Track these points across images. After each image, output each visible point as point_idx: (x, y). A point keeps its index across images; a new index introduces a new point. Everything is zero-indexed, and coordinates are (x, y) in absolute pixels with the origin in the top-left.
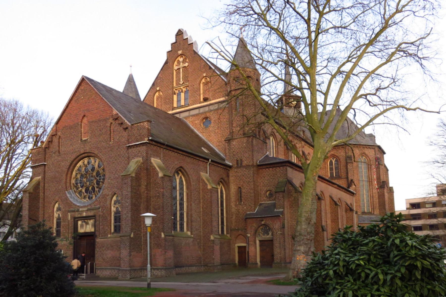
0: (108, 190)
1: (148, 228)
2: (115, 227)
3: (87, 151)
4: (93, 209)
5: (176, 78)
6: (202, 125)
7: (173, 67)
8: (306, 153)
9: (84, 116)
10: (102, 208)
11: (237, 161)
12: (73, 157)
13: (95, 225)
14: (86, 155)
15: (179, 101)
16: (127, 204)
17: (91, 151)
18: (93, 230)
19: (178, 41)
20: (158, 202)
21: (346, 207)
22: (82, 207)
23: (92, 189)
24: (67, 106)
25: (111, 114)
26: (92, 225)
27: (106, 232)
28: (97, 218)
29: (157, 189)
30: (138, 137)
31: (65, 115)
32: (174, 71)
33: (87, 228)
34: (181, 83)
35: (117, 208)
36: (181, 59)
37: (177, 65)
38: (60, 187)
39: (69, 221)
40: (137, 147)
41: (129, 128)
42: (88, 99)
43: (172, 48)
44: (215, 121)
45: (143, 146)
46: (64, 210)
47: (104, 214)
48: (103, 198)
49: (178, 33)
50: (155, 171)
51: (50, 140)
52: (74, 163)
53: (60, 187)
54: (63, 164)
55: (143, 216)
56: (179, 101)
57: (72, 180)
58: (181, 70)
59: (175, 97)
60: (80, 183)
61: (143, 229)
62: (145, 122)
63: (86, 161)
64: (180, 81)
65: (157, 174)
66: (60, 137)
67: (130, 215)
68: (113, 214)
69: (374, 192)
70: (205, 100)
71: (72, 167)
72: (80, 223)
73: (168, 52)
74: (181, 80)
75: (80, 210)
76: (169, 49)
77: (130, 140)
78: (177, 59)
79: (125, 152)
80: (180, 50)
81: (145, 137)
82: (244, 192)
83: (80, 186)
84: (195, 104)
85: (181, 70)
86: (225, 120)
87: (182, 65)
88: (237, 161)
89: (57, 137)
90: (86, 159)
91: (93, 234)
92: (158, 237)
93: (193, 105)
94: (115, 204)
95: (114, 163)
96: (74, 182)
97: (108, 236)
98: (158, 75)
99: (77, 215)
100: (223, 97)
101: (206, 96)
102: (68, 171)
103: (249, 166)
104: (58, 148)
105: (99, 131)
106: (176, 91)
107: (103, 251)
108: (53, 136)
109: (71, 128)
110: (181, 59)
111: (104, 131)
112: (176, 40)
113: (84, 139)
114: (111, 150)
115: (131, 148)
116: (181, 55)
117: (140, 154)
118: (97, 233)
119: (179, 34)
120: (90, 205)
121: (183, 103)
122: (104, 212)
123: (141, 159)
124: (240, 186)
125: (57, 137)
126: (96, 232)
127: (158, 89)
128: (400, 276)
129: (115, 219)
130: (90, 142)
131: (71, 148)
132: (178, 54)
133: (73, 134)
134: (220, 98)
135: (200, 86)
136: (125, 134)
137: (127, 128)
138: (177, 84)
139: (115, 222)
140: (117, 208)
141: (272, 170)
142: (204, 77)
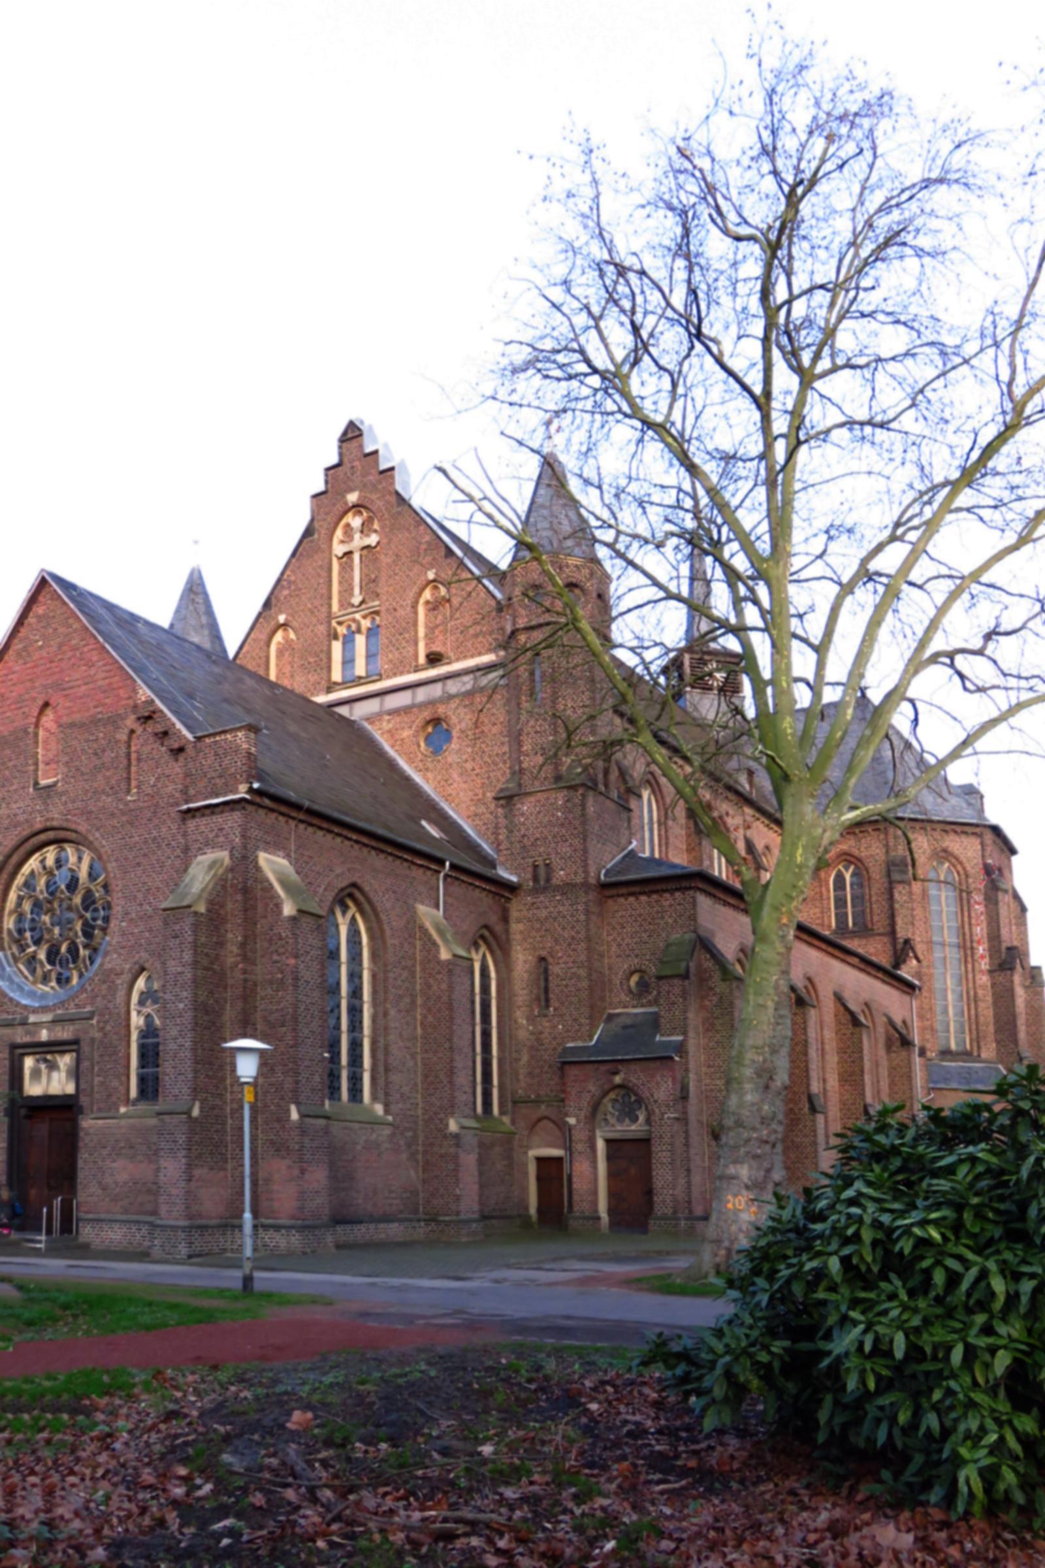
2: (142, 1080)
3: (55, 824)
6: (422, 744)
8: (759, 846)
9: (46, 705)
11: (536, 867)
13: (76, 1073)
15: (348, 662)
16: (181, 1006)
18: (70, 1089)
19: (345, 460)
21: (887, 1032)
22: (35, 1011)
23: (69, 950)
25: (131, 702)
26: (69, 1073)
27: (114, 1099)
28: (85, 1048)
29: (275, 957)
34: (356, 600)
37: (342, 542)
41: (190, 750)
42: (60, 646)
43: (326, 482)
44: (462, 731)
45: (232, 810)
48: (104, 982)
49: (345, 433)
56: (348, 662)
59: (337, 647)
62: (239, 729)
63: (50, 854)
64: (352, 595)
65: (278, 907)
67: (188, 1044)
68: (134, 1036)
70: (434, 659)
72: (29, 1062)
73: (315, 496)
74: (357, 590)
77: (192, 792)
80: (351, 490)
81: (237, 782)
83: (29, 941)
84: (402, 673)
85: (356, 557)
86: (495, 730)
87: (358, 541)
88: (536, 867)
90: (51, 848)
92: (278, 1120)
93: (395, 675)
94: (141, 1003)
97: (117, 1110)
98: (283, 574)
100: (489, 651)
101: (436, 648)
105: (94, 758)
107: (103, 1160)
110: (356, 522)
111: (109, 755)
112: (341, 455)
113: (44, 782)
114: (131, 823)
115: (194, 817)
116: (357, 507)
117: (221, 839)
118: (84, 1100)
120: (63, 1003)
121: (360, 669)
124: (544, 953)
127: (282, 619)
129: (142, 1056)
132: (346, 503)
133: (10, 764)
134: (480, 654)
135: (416, 613)
136: (176, 768)
137: (181, 750)
141: (649, 903)
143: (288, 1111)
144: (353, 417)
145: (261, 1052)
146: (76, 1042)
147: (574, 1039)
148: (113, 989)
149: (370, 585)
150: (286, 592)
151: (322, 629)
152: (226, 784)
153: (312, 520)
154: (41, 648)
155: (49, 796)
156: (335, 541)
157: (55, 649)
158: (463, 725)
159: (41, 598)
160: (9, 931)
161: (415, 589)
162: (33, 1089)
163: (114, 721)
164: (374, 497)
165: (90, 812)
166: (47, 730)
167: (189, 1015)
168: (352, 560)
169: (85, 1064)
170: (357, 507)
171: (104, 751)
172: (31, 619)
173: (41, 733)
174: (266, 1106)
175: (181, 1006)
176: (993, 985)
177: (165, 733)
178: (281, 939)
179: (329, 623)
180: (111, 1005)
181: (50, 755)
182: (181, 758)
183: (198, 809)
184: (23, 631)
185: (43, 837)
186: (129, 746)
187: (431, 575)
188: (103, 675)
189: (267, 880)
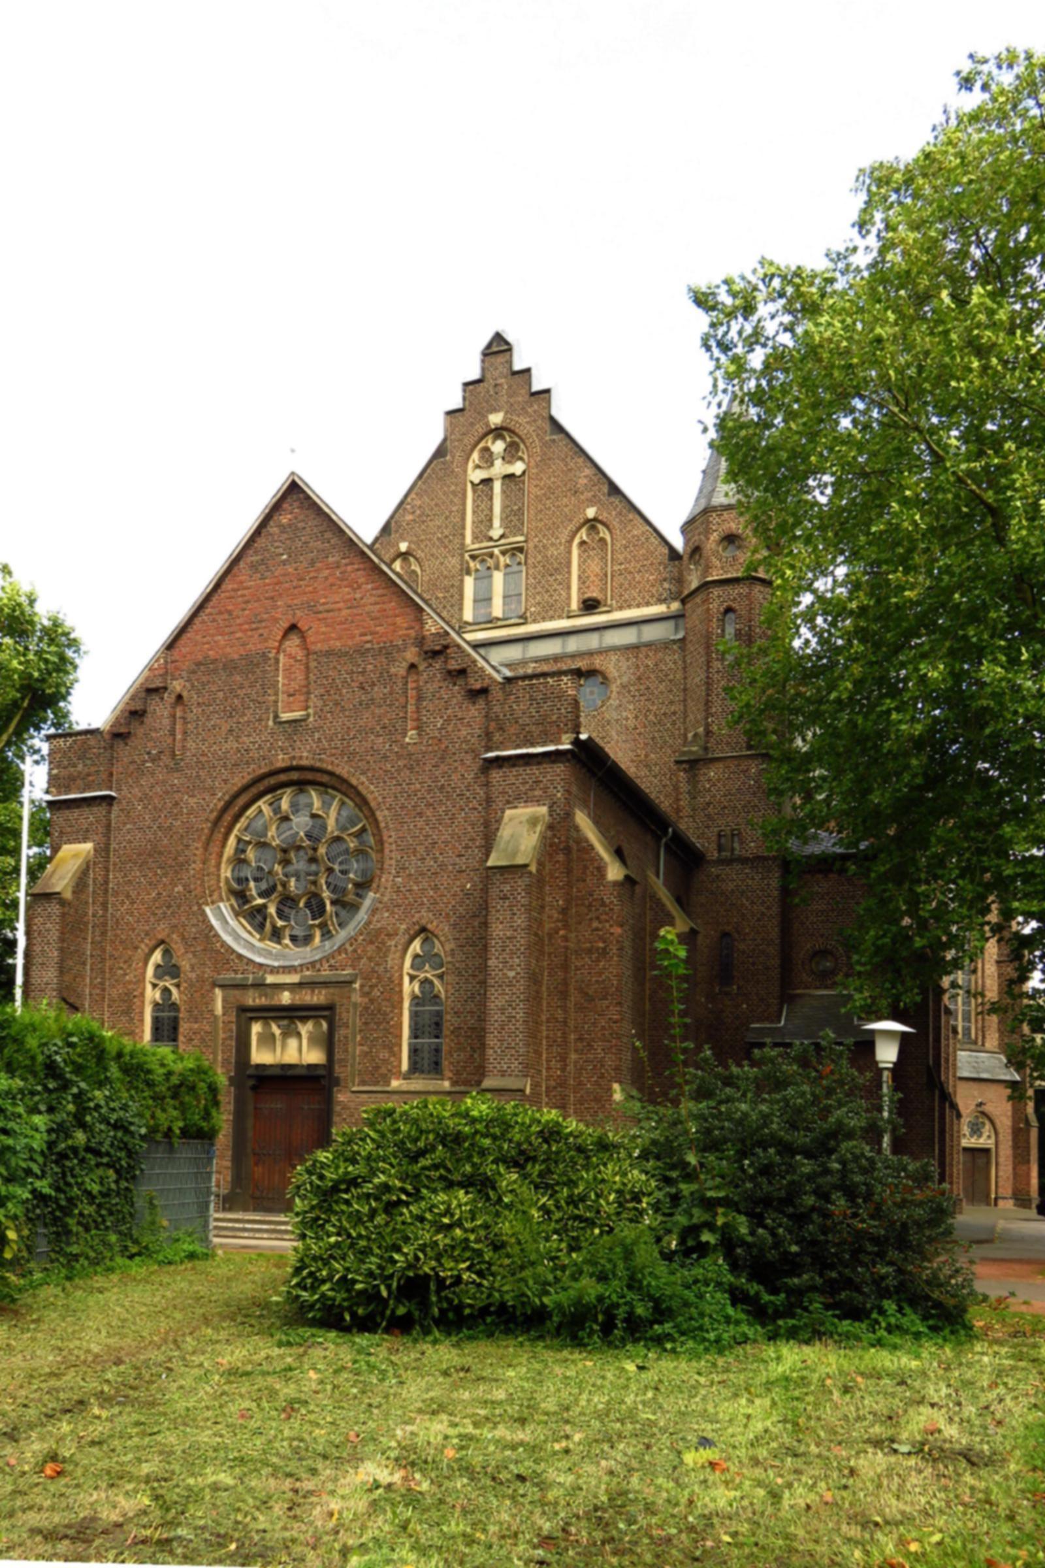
0: (393, 913)
1: (886, 1074)
2: (414, 1051)
3: (304, 762)
4: (325, 984)
5: (474, 512)
7: (465, 471)
9: (293, 628)
10: (367, 978)
12: (238, 781)
14: (295, 776)
15: (483, 599)
16: (512, 974)
17: (318, 764)
18: (314, 1057)
19: (488, 376)
20: (600, 974)
22: (274, 970)
24: (218, 585)
27: (383, 1070)
29: (595, 924)
30: (533, 728)
31: (203, 616)
32: (469, 486)
33: (299, 1050)
34: (496, 533)
35: (425, 982)
36: (498, 447)
37: (478, 467)
38: (180, 888)
39: (216, 1017)
40: (527, 764)
41: (496, 694)
42: (312, 563)
43: (464, 399)
44: (623, 686)
45: (554, 762)
46: (193, 976)
47: (372, 1001)
48: (372, 942)
49: (489, 346)
50: (592, 860)
51: (138, 706)
52: (241, 801)
53: (180, 888)
54: (192, 801)
55: (873, 1032)
56: (483, 599)
57: (223, 866)
58: (497, 486)
59: (469, 582)
60: (256, 880)
61: (548, 1069)
62: (565, 673)
64: (491, 526)
65: (601, 870)
66: (180, 697)
67: (520, 1015)
68: (406, 1004)
69: (987, 972)
70: (590, 606)
71: (228, 818)
72: (256, 1028)
73: (449, 413)
75: (270, 979)
76: (455, 400)
77: (497, 737)
78: (482, 445)
79: (470, 777)
80: (495, 410)
81: (560, 731)
82: (744, 952)
83: (254, 892)
84: (552, 618)
85: (497, 486)
87: (499, 468)
89: (169, 698)
90: (289, 790)
91: (322, 1072)
92: (597, 1100)
93: (544, 619)
95: (420, 814)
96: (229, 874)
98: (406, 496)
99: (252, 999)
100: (661, 601)
101: (595, 594)
102: (212, 831)
103: (765, 859)
104: (169, 740)
105: (358, 693)
106: (472, 564)
108: (150, 691)
109: (230, 667)
110: (498, 447)
111: (378, 691)
112: (483, 369)
113: (285, 716)
114: (411, 768)
115: (500, 767)
116: (498, 432)
117: (538, 793)
119: (495, 349)
120: (313, 964)
121: (497, 610)
122: (376, 993)
123: (544, 810)
124: (728, 928)
125: (169, 698)
126: (337, 1069)
127: (403, 547)
128: (27, 1196)
130: (317, 729)
131: (232, 744)
132: (487, 424)
133: (241, 692)
134: (648, 604)
135: (570, 552)
136: (474, 712)
137: (484, 691)
138: (476, 538)
139: (415, 1035)
140: (425, 982)
142: (588, 521)
143: (610, 1090)
144: (500, 330)
145: (904, 1034)
146: (330, 1008)
147: (759, 1021)
148: (383, 951)
149: (513, 519)
150: (409, 517)
151: (455, 561)
152: (545, 733)
153: (445, 440)
154: (284, 563)
155: (295, 732)
156: (471, 465)
157: (305, 564)
158: (625, 679)
159: (285, 506)
160: (227, 879)
161: (572, 527)
162: (260, 1056)
163: (388, 652)
164: (523, 420)
165: (354, 753)
166: (290, 656)
167: (521, 986)
168: (491, 489)
169: (340, 1033)
170: (498, 432)
171: (373, 684)
172: (273, 528)
173: (281, 657)
174: (580, 1083)
175: (512, 974)
176: (1000, 975)
177: (462, 672)
178: (603, 904)
179: (462, 556)
180: (381, 969)
181: (294, 685)
182: (481, 703)
183: (509, 758)
184: (261, 542)
185: (283, 777)
186: (406, 683)
187: (591, 513)
188: (373, 600)
189: (587, 840)
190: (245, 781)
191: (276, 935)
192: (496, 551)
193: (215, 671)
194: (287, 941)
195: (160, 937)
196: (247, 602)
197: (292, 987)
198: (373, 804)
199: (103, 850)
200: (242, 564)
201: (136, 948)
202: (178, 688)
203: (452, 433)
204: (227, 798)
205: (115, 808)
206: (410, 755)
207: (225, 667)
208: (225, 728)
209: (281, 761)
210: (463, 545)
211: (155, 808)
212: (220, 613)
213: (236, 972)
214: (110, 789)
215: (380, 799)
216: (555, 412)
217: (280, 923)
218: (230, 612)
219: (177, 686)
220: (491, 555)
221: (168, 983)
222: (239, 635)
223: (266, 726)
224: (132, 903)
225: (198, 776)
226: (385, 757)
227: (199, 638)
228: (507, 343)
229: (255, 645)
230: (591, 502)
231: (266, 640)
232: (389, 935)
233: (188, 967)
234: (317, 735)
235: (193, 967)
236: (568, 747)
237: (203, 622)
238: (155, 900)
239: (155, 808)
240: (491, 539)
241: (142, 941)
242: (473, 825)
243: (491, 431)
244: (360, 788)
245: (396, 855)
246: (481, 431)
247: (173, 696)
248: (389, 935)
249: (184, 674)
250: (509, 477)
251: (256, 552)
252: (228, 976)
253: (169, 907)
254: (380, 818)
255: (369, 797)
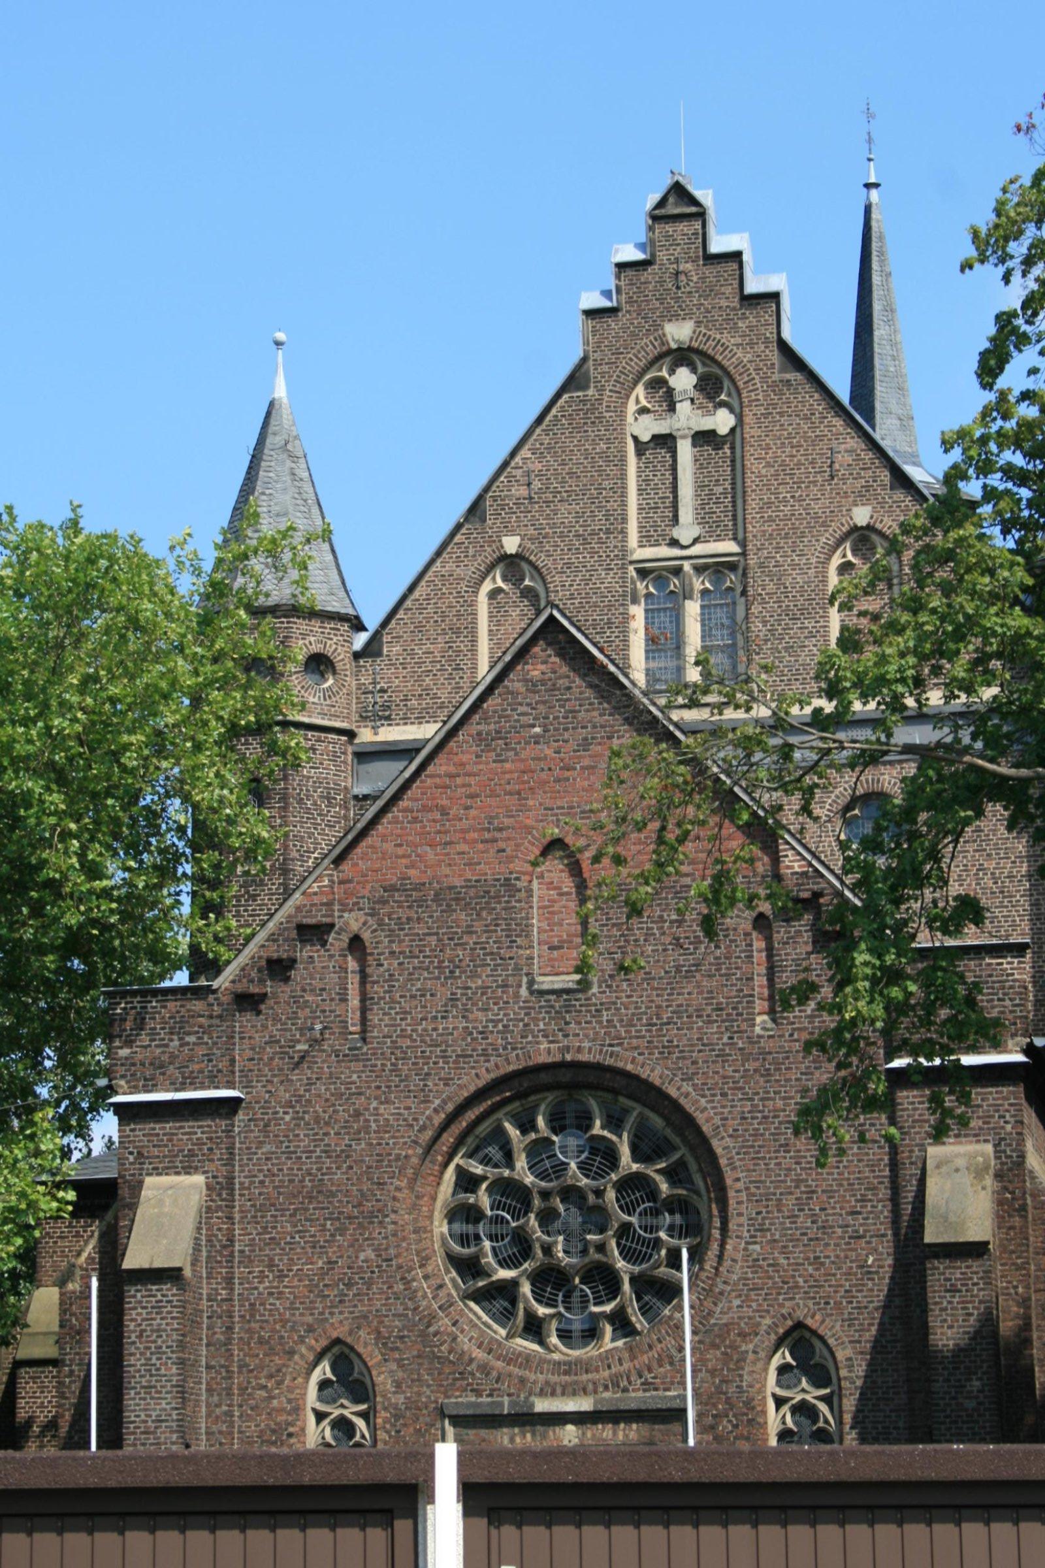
5: (640, 490)
7: (622, 416)
14: (566, 1076)
19: (662, 256)
38: (370, 1253)
48: (715, 1346)
49: (661, 204)
52: (471, 1115)
85: (685, 449)
87: (688, 418)
89: (337, 942)
106: (640, 586)
110: (683, 380)
113: (547, 982)
116: (682, 356)
123: (989, 1148)
127: (511, 545)
133: (471, 940)
138: (646, 539)
142: (856, 529)
153: (584, 360)
156: (632, 407)
166: (550, 885)
170: (682, 356)
185: (544, 1078)
190: (481, 1083)
191: (534, 1328)
192: (687, 566)
193: (421, 902)
194: (554, 1340)
195: (335, 1335)
196: (472, 796)
197: (579, 1418)
198: (706, 1129)
199: (222, 1190)
200: (461, 736)
201: (291, 1353)
202: (355, 926)
203: (598, 345)
204: (450, 1107)
205: (241, 1115)
206: (764, 1053)
207: (437, 898)
208: (443, 993)
209: (544, 1052)
210: (624, 550)
211: (317, 1120)
212: (425, 809)
213: (478, 1393)
214: (230, 1085)
215: (717, 1121)
216: (786, 335)
217: (542, 1311)
218: (444, 812)
219: (353, 921)
220: (677, 571)
221: (350, 1410)
222: (464, 847)
223: (517, 995)
224: (281, 1276)
225: (395, 1069)
226: (722, 1055)
227: (389, 847)
228: (694, 201)
229: (490, 868)
230: (863, 496)
231: (510, 859)
232: (743, 1335)
233: (390, 1387)
234: (605, 1016)
235: (398, 1385)
236: (1020, 1058)
237: (396, 821)
238: (323, 1273)
239: (317, 1120)
240: (674, 543)
241: (302, 1340)
242: (872, 1167)
243: (670, 352)
244: (682, 1101)
245: (748, 1209)
246: (652, 352)
247: (346, 938)
248: (743, 1335)
249: (364, 902)
250: (704, 438)
251: (485, 719)
252: (464, 1401)
253: (349, 1285)
254: (719, 1151)
255: (700, 1118)
